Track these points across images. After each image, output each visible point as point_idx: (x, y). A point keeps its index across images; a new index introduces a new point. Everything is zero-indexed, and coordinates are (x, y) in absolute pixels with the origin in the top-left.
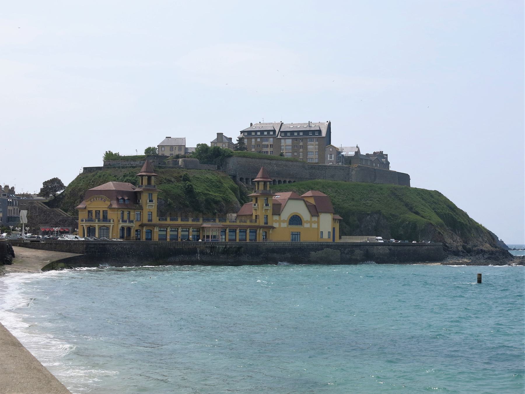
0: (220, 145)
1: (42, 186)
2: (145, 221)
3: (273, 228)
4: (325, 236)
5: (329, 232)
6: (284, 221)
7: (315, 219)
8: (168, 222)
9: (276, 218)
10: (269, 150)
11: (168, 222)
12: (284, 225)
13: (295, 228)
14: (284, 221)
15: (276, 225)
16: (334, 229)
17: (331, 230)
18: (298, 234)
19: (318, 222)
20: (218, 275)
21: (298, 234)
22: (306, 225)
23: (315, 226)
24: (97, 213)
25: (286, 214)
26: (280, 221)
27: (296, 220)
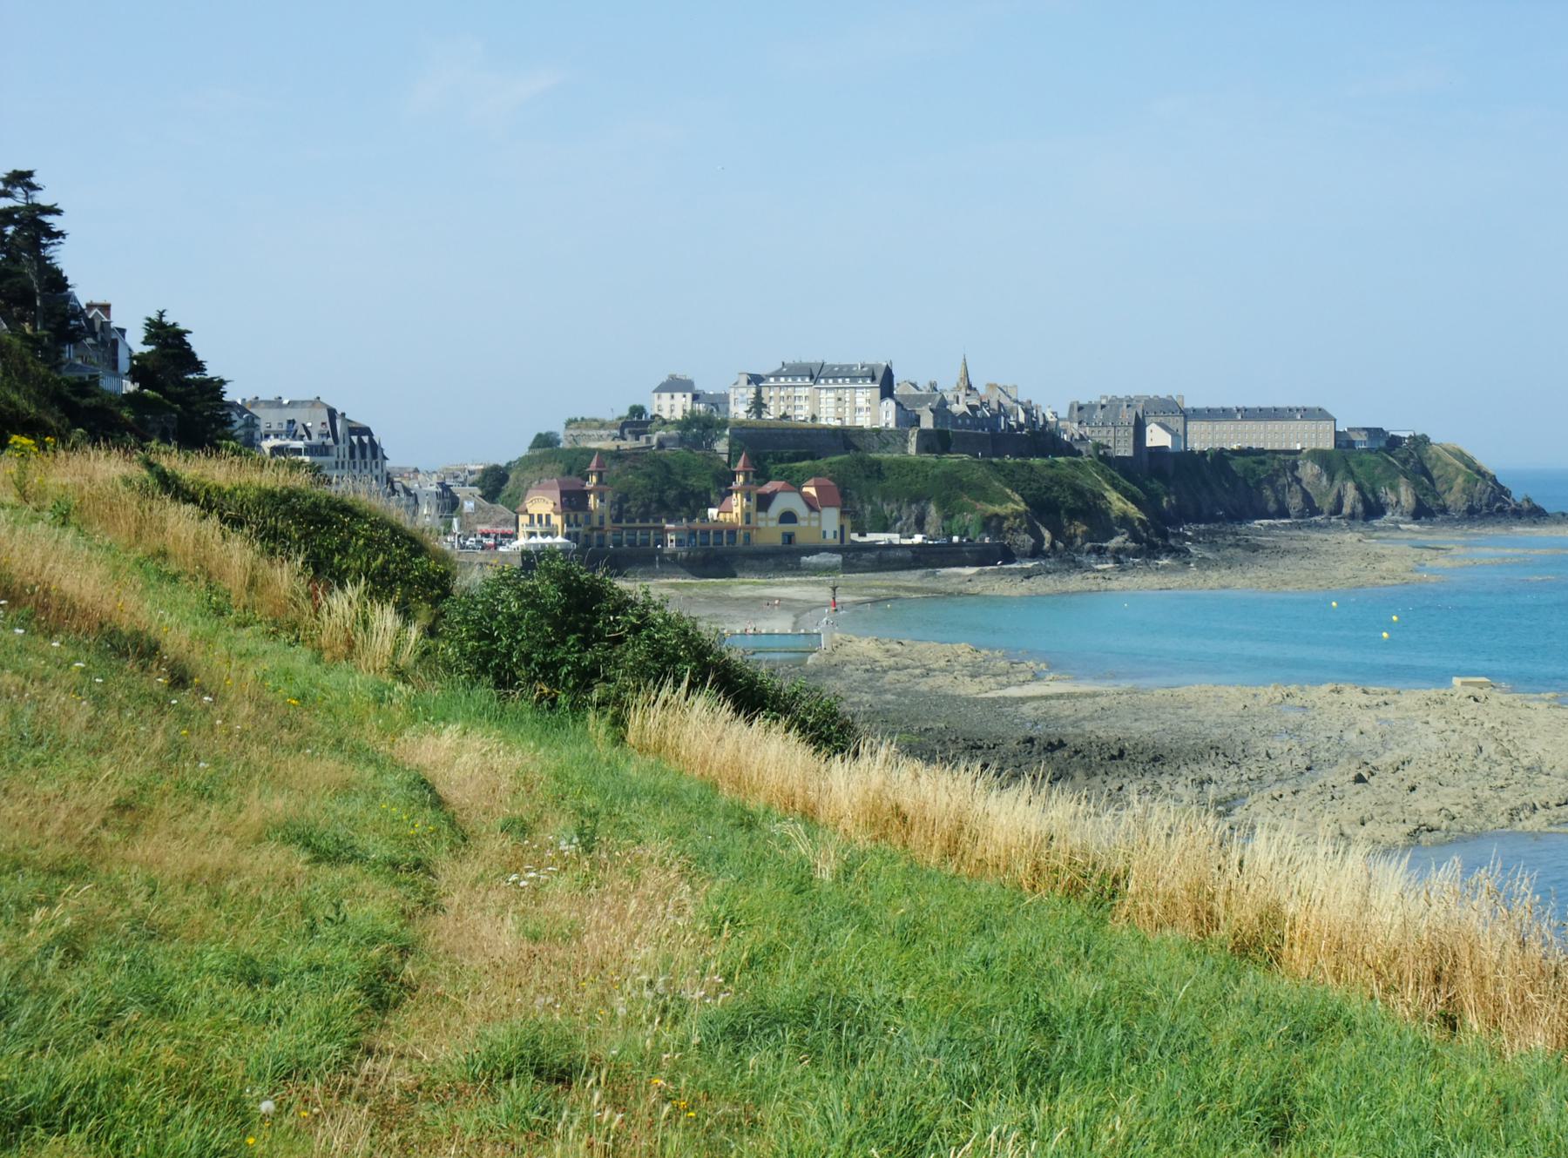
0: (441, 770)
1: (200, 358)
3: (758, 529)
4: (830, 536)
7: (814, 515)
8: (651, 523)
9: (761, 515)
10: (69, 920)
11: (638, 524)
12: (773, 524)
13: (788, 527)
15: (762, 524)
16: (842, 527)
19: (820, 519)
20: (1380, 557)
22: (803, 523)
23: (815, 524)
25: (776, 508)
26: (766, 520)
27: (788, 517)
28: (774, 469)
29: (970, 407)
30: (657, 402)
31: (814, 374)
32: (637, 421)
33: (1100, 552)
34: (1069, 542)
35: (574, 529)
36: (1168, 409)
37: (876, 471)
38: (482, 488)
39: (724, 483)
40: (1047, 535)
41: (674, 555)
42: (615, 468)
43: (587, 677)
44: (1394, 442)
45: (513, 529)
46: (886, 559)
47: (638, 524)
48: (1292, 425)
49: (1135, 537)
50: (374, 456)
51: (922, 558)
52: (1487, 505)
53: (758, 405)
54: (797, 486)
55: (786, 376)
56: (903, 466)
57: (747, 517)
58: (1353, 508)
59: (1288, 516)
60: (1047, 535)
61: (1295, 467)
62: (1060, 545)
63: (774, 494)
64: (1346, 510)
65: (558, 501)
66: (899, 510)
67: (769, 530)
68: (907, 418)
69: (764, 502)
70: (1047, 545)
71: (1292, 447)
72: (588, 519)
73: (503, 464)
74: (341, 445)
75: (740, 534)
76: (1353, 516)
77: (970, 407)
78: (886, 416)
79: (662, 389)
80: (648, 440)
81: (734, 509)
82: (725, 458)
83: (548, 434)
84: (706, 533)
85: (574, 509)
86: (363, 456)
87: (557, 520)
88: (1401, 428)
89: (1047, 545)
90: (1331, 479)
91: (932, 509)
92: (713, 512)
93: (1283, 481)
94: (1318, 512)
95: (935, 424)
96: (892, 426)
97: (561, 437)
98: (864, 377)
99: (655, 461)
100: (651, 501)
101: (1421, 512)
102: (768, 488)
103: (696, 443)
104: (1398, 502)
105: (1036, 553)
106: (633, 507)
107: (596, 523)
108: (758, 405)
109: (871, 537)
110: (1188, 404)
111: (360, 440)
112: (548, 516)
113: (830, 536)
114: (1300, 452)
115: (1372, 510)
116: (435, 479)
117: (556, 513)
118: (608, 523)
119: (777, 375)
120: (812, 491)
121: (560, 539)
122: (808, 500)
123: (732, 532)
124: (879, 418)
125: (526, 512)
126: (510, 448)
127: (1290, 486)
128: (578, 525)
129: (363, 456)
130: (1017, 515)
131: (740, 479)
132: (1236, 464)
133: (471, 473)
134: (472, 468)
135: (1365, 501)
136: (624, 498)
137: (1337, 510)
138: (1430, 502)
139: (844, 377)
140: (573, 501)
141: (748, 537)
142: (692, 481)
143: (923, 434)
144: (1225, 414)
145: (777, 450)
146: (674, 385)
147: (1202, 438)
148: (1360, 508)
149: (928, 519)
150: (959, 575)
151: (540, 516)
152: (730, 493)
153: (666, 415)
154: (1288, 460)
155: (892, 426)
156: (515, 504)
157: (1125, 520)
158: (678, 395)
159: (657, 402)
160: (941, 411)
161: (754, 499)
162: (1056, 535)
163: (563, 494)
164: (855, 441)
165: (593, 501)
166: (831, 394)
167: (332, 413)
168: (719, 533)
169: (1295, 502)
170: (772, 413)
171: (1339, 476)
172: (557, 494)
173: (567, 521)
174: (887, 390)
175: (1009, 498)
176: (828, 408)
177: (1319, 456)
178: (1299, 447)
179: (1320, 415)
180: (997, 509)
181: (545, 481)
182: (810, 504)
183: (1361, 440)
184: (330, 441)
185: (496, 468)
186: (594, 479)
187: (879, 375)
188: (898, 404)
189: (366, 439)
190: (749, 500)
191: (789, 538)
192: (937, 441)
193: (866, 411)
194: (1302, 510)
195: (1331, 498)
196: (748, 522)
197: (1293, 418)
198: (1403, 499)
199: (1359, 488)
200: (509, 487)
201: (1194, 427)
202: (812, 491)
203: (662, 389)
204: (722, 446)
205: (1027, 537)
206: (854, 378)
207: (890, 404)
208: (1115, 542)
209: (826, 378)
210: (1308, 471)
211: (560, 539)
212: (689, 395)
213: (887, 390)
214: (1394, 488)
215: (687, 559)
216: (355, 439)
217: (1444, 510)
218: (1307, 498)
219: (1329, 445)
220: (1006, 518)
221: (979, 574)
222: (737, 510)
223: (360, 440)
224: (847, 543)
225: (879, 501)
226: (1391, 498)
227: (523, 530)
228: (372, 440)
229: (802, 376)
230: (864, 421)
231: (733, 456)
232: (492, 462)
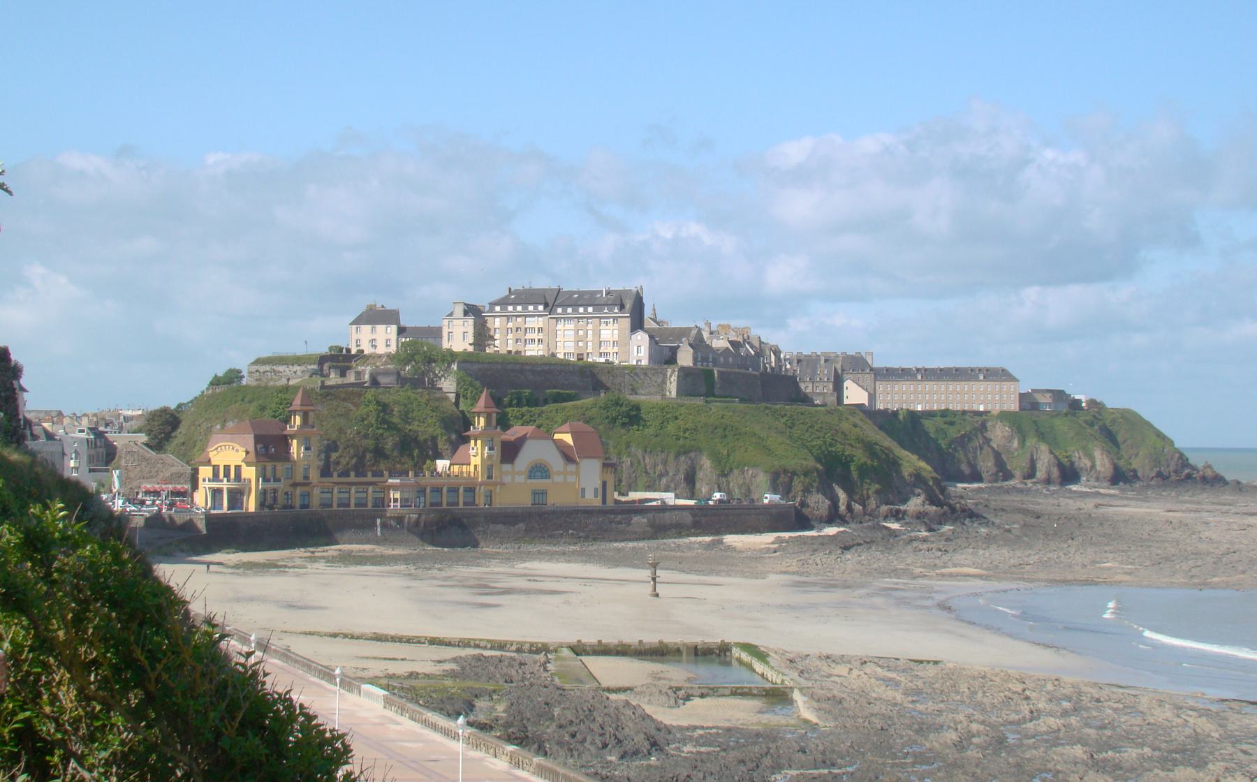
2: (299, 479)
3: (503, 484)
4: (589, 495)
5: (596, 490)
6: (520, 473)
7: (572, 467)
9: (507, 467)
11: (353, 478)
12: (521, 479)
13: (539, 483)
14: (520, 473)
15: (507, 479)
16: (604, 484)
17: (598, 484)
18: (543, 493)
19: (577, 473)
21: (543, 493)
22: (558, 479)
24: (227, 468)
27: (539, 470)
29: (731, 343)
30: (355, 336)
31: (552, 302)
35: (272, 485)
36: (857, 365)
37: (634, 417)
38: (149, 433)
39: (459, 431)
40: (842, 495)
41: (400, 519)
42: (323, 409)
43: (159, 609)
44: (1075, 404)
45: (187, 486)
47: (353, 478)
48: (975, 386)
49: (932, 500)
52: (1176, 472)
53: (482, 335)
55: (515, 304)
56: (667, 413)
57: (489, 469)
58: (1049, 473)
59: (980, 480)
60: (842, 495)
61: (983, 427)
62: (857, 507)
63: (521, 441)
64: (1041, 474)
65: (252, 449)
66: (665, 462)
67: (515, 489)
68: (664, 356)
69: (510, 452)
70: (842, 508)
71: (975, 408)
72: (290, 473)
73: (173, 406)
75: (481, 492)
76: (1048, 481)
77: (731, 343)
78: (638, 351)
80: (358, 374)
81: (476, 455)
82: (452, 397)
83: (231, 371)
84: (437, 490)
85: (273, 458)
89: (842, 508)
91: (706, 463)
92: (441, 464)
93: (976, 443)
95: (695, 360)
96: (645, 362)
97: (245, 373)
98: (610, 305)
100: (366, 450)
103: (416, 382)
104: (1093, 466)
106: (344, 458)
107: (299, 478)
108: (482, 335)
109: (634, 496)
110: (877, 364)
112: (238, 468)
113: (589, 495)
114: (986, 413)
116: (85, 423)
117: (248, 464)
118: (314, 475)
119: (504, 302)
120: (568, 438)
122: (562, 448)
123: (471, 490)
124: (628, 353)
125: (208, 462)
126: (180, 388)
127: (981, 449)
128: (277, 480)
131: (481, 422)
132: (928, 425)
133: (127, 419)
134: (129, 413)
135: (1060, 465)
136: (332, 447)
137: (1031, 474)
139: (586, 306)
140: (270, 448)
141: (489, 496)
142: (415, 426)
143: (685, 373)
144: (904, 374)
145: (522, 390)
146: (373, 316)
147: (894, 398)
148: (1055, 472)
149: (700, 475)
150: (690, 547)
151: (227, 468)
152: (466, 440)
153: (368, 350)
154: (980, 421)
155: (645, 362)
156: (193, 455)
157: (918, 478)
158: (381, 328)
159: (355, 336)
160: (699, 345)
161: (498, 448)
162: (850, 492)
163: (258, 439)
164: (604, 379)
165: (295, 448)
166: (571, 326)
168: (454, 490)
169: (986, 465)
172: (250, 439)
173: (262, 474)
174: (637, 323)
176: (565, 339)
177: (1004, 416)
178: (982, 408)
181: (230, 424)
182: (567, 455)
183: (1045, 400)
185: (165, 411)
186: (298, 420)
187: (628, 305)
188: (651, 337)
190: (491, 449)
191: (540, 494)
192: (699, 382)
193: (611, 343)
194: (996, 474)
195: (1024, 463)
196: (490, 477)
197: (976, 379)
198: (1098, 463)
200: (181, 434)
202: (568, 438)
203: (358, 321)
204: (448, 385)
205: (820, 497)
206: (598, 306)
207: (641, 338)
208: (915, 504)
209: (565, 306)
210: (999, 434)
212: (394, 328)
215: (417, 523)
219: (1014, 407)
221: (781, 546)
222: (476, 461)
224: (610, 503)
225: (640, 453)
226: (1086, 463)
229: (536, 304)
232: (156, 405)
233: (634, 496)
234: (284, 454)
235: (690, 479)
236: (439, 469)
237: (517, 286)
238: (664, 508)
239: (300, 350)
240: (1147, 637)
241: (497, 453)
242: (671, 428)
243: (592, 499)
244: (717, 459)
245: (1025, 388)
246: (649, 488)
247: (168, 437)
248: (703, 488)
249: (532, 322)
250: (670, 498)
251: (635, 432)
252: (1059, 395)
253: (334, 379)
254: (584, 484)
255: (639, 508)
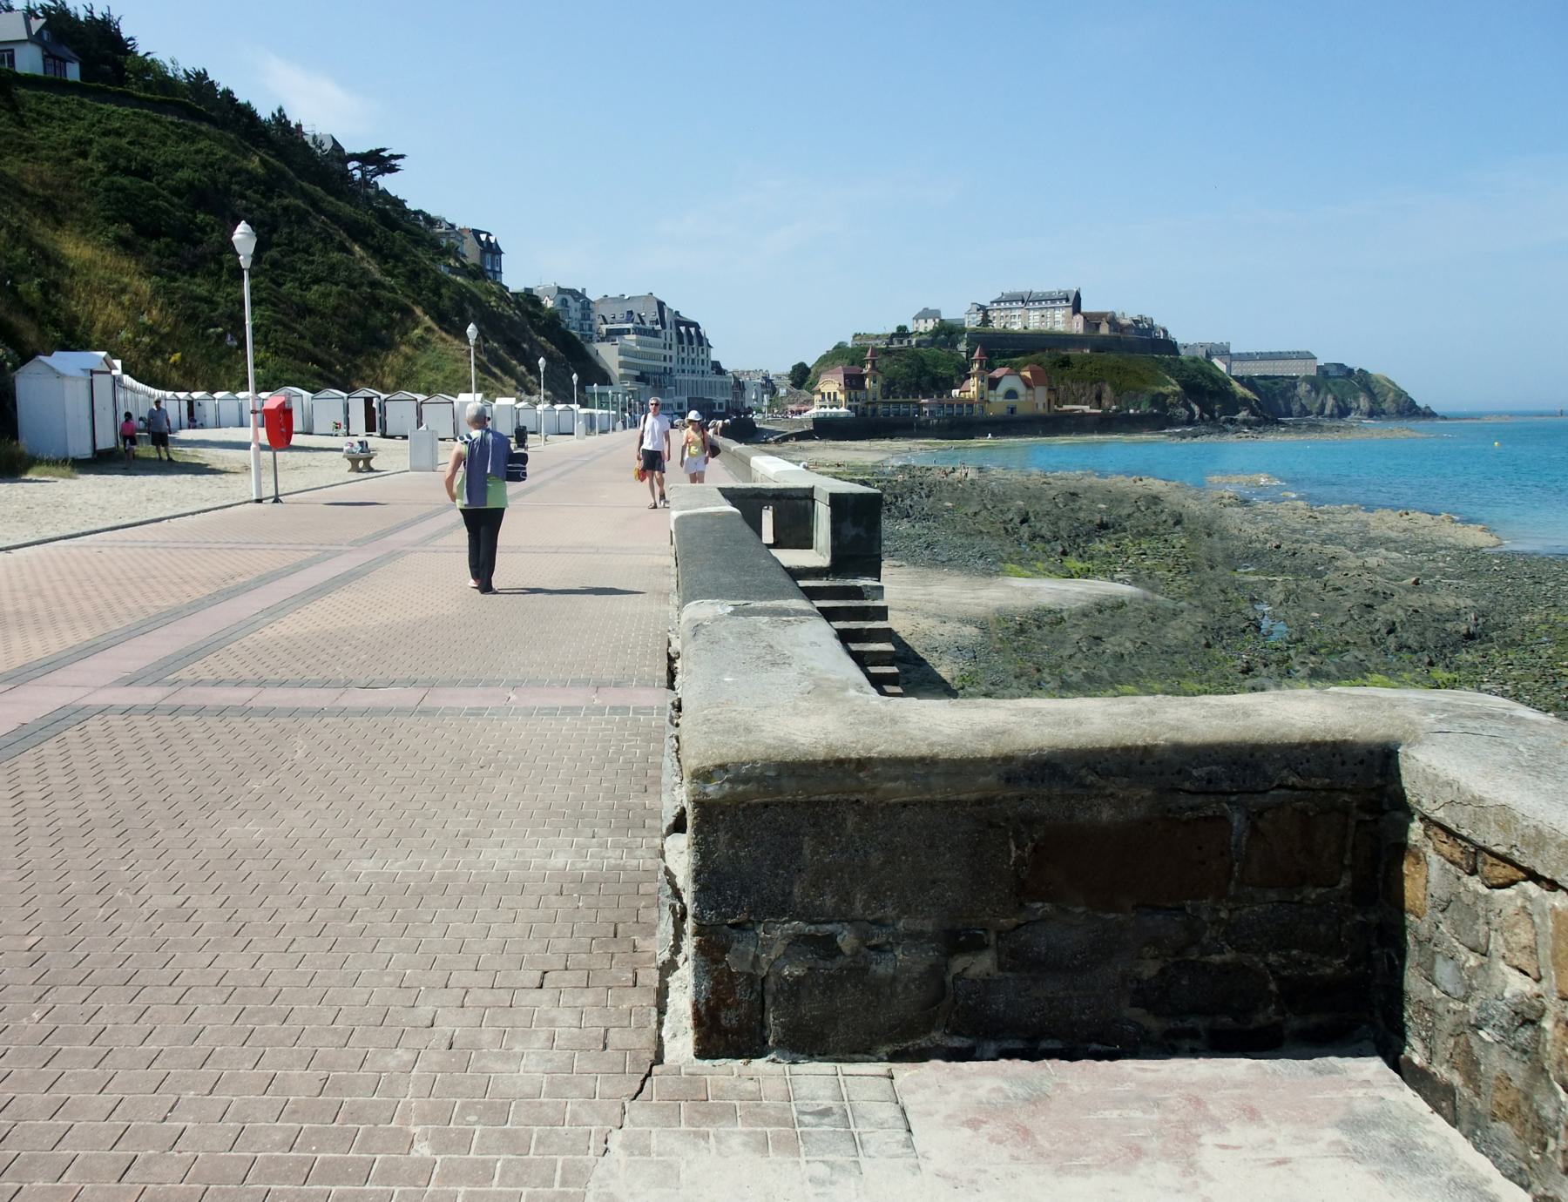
4: (1041, 407)
12: (1000, 399)
13: (1011, 402)
22: (1022, 399)
25: (1002, 388)
27: (1011, 394)
28: (998, 362)
32: (902, 332)
33: (1232, 422)
34: (1212, 413)
36: (1224, 352)
37: (1066, 363)
40: (1196, 409)
42: (885, 361)
44: (1351, 371)
46: (1079, 425)
48: (1290, 362)
49: (1253, 413)
50: (700, 344)
51: (1105, 424)
53: (986, 321)
54: (1017, 372)
60: (1196, 409)
64: (1327, 412)
67: (998, 403)
69: (994, 384)
74: (668, 330)
76: (1331, 416)
79: (916, 318)
81: (973, 387)
84: (951, 406)
85: (853, 388)
86: (691, 343)
87: (841, 397)
88: (1354, 363)
90: (1318, 393)
91: (1108, 388)
92: (955, 392)
94: (1310, 413)
99: (915, 356)
101: (1371, 414)
102: (997, 373)
105: (1190, 422)
108: (986, 321)
109: (1066, 407)
111: (688, 332)
113: (1041, 407)
115: (1343, 412)
120: (1028, 374)
121: (843, 410)
122: (1024, 380)
123: (970, 404)
129: (691, 343)
130: (1175, 394)
137: (1321, 412)
138: (1376, 407)
140: (853, 382)
141: (983, 408)
145: (999, 348)
154: (1293, 382)
157: (1245, 401)
162: (1203, 410)
163: (846, 376)
167: (661, 305)
168: (960, 406)
169: (1296, 407)
170: (997, 325)
171: (1323, 391)
175: (1169, 383)
177: (1308, 379)
179: (1308, 356)
180: (1161, 389)
182: (1027, 384)
183: (1333, 372)
184: (659, 327)
187: (1072, 299)
189: (693, 330)
193: (1060, 321)
199: (1335, 398)
201: (1235, 364)
202: (1028, 374)
204: (962, 347)
207: (1079, 318)
208: (1242, 415)
211: (843, 410)
213: (1077, 308)
214: (1356, 399)
216: (683, 329)
217: (1383, 412)
218: (1303, 406)
220: (1167, 396)
222: (974, 389)
223: (688, 332)
226: (1354, 405)
227: (817, 403)
228: (698, 333)
230: (1060, 327)
231: (970, 353)
233: (1066, 407)
234: (861, 386)
235: (1099, 398)
236: (69, 65)
237: (1006, 291)
238: (1083, 414)
239: (880, 332)
240: (1558, 900)
241: (986, 385)
242: (1087, 368)
243: (1041, 409)
244: (1113, 385)
245: (1321, 362)
246: (1075, 403)
247: (803, 381)
248: (1106, 403)
249: (1017, 313)
250: (1087, 408)
251: (1067, 371)
252: (1341, 366)
253: (896, 345)
254: (1035, 401)
255: (1070, 415)
